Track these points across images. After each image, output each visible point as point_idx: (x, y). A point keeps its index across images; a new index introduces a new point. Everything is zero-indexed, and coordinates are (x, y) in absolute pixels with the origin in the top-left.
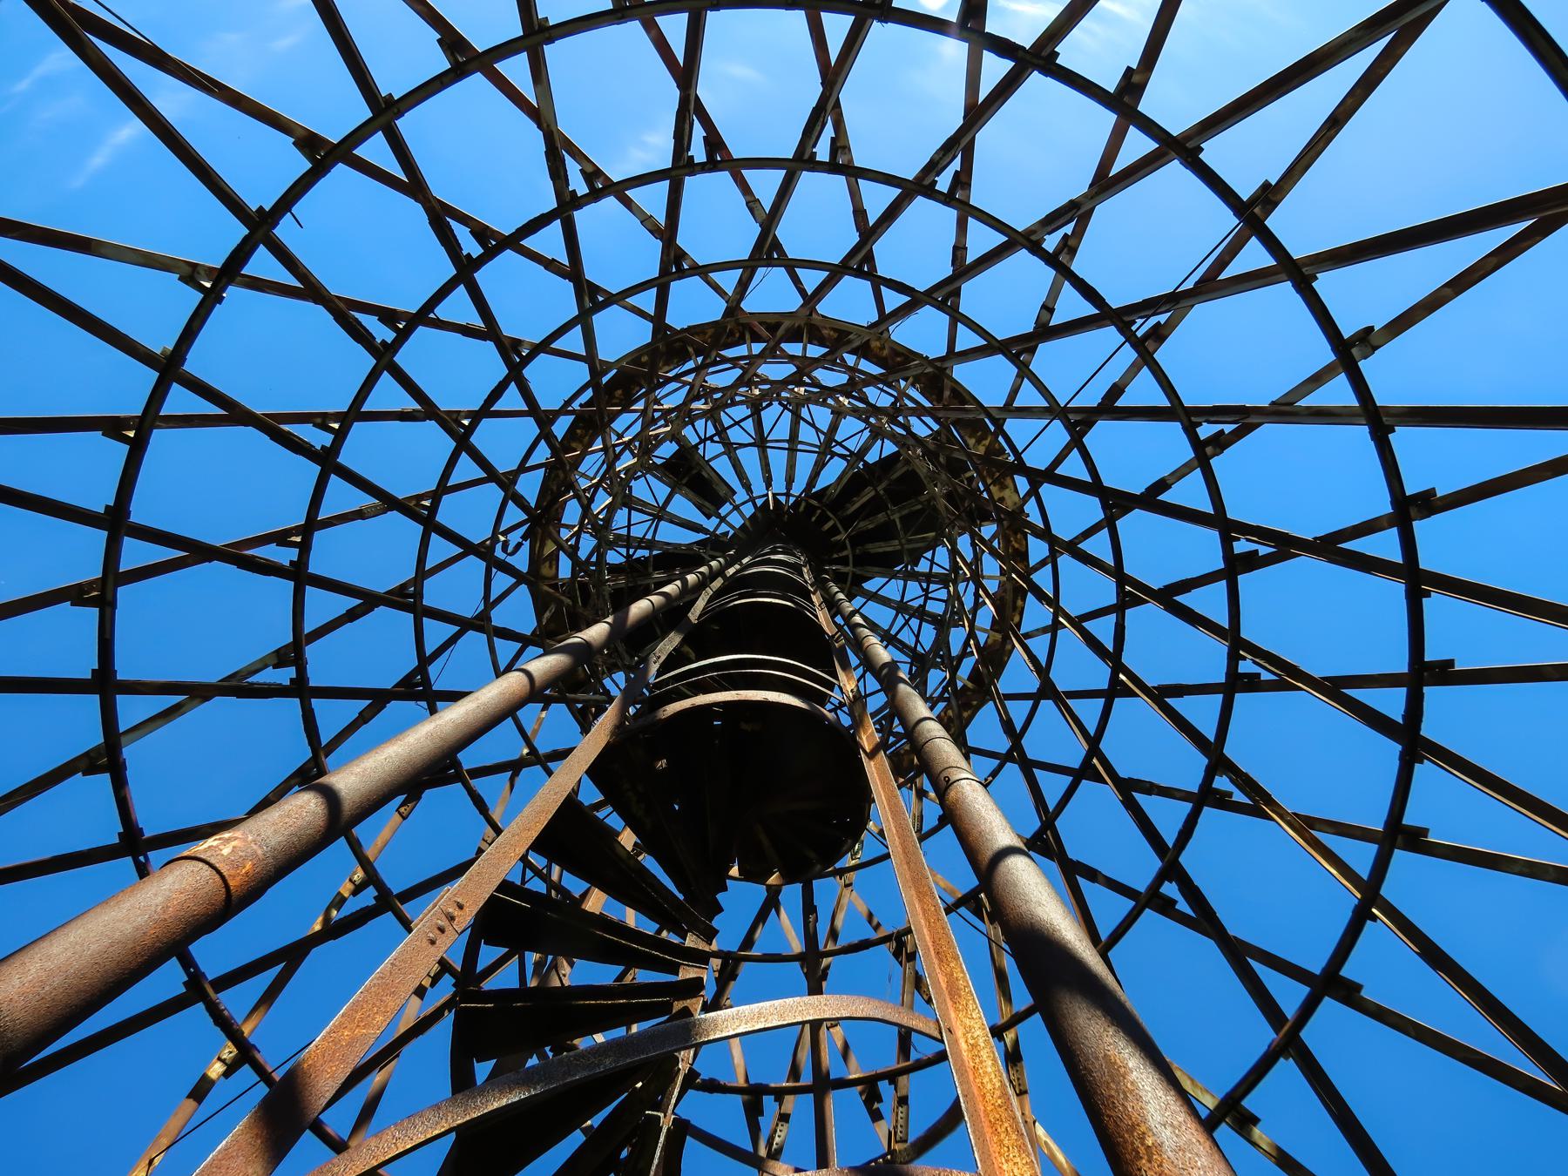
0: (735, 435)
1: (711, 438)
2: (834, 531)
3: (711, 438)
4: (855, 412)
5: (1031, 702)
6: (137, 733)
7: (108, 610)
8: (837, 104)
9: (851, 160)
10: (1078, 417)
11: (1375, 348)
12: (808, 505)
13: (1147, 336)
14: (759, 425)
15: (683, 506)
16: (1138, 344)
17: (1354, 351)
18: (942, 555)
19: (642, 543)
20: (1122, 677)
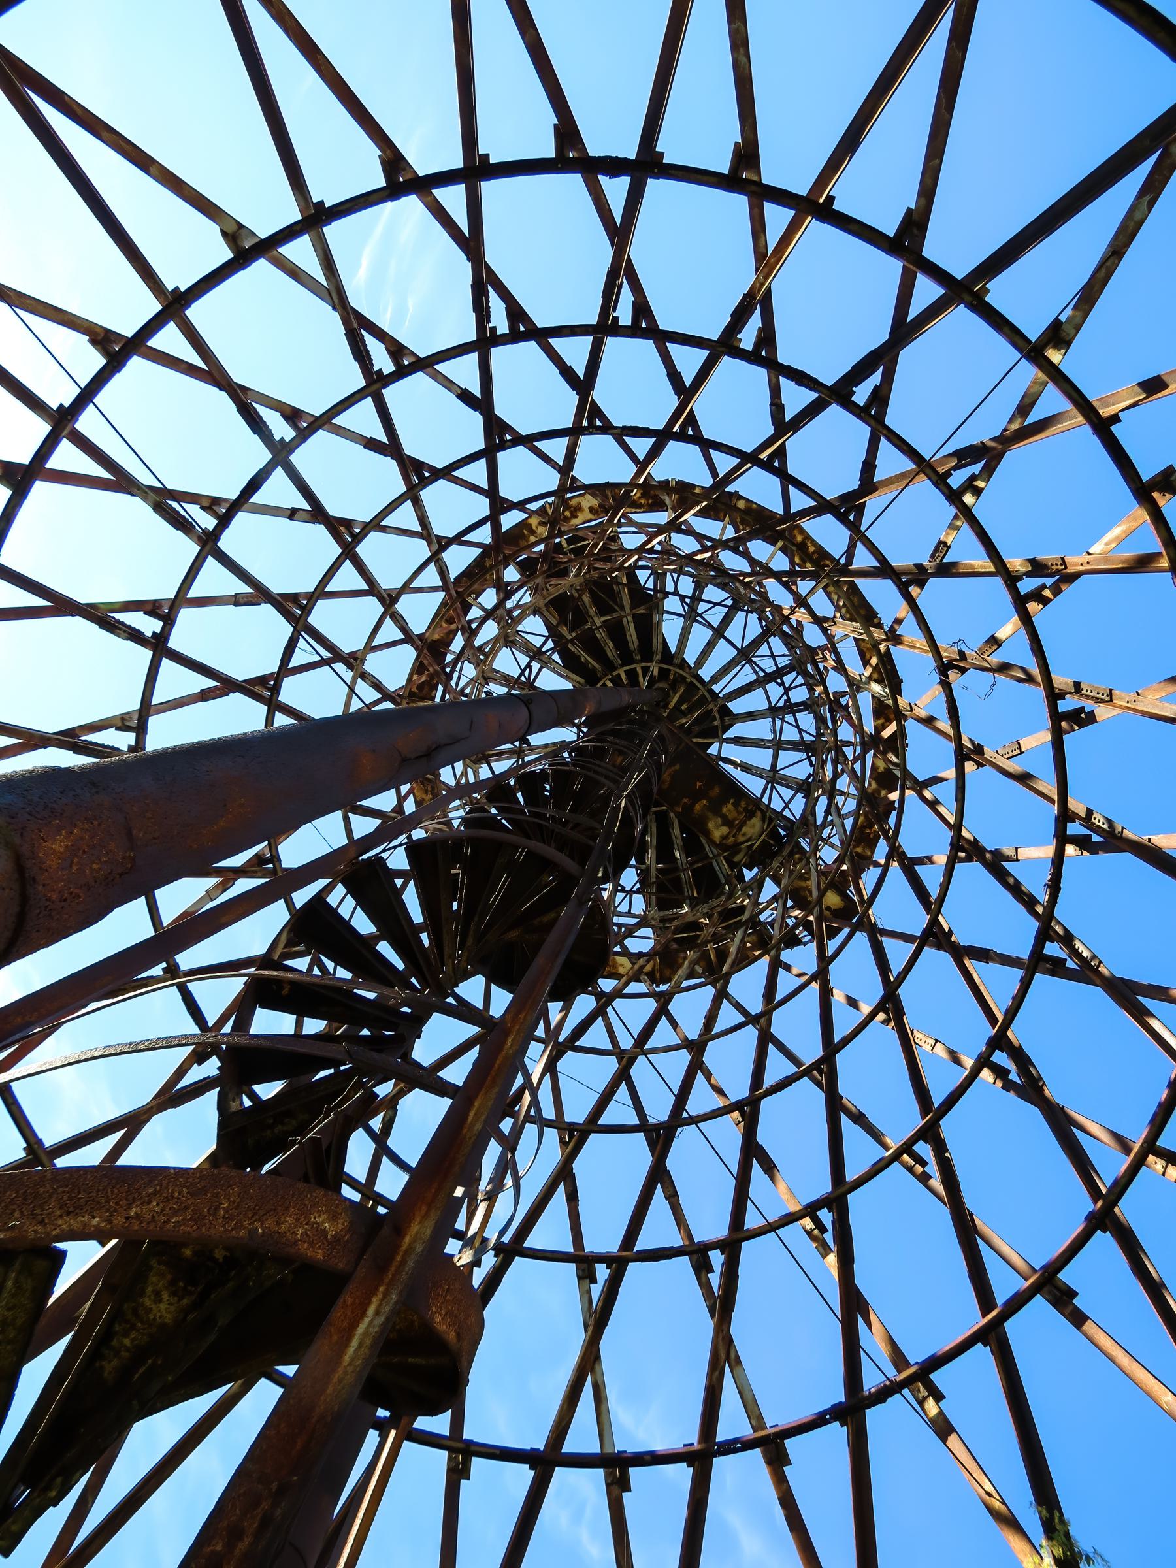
6: (606, 1427)
7: (473, 1448)
11: (241, 226)
17: (247, 245)
20: (676, 428)
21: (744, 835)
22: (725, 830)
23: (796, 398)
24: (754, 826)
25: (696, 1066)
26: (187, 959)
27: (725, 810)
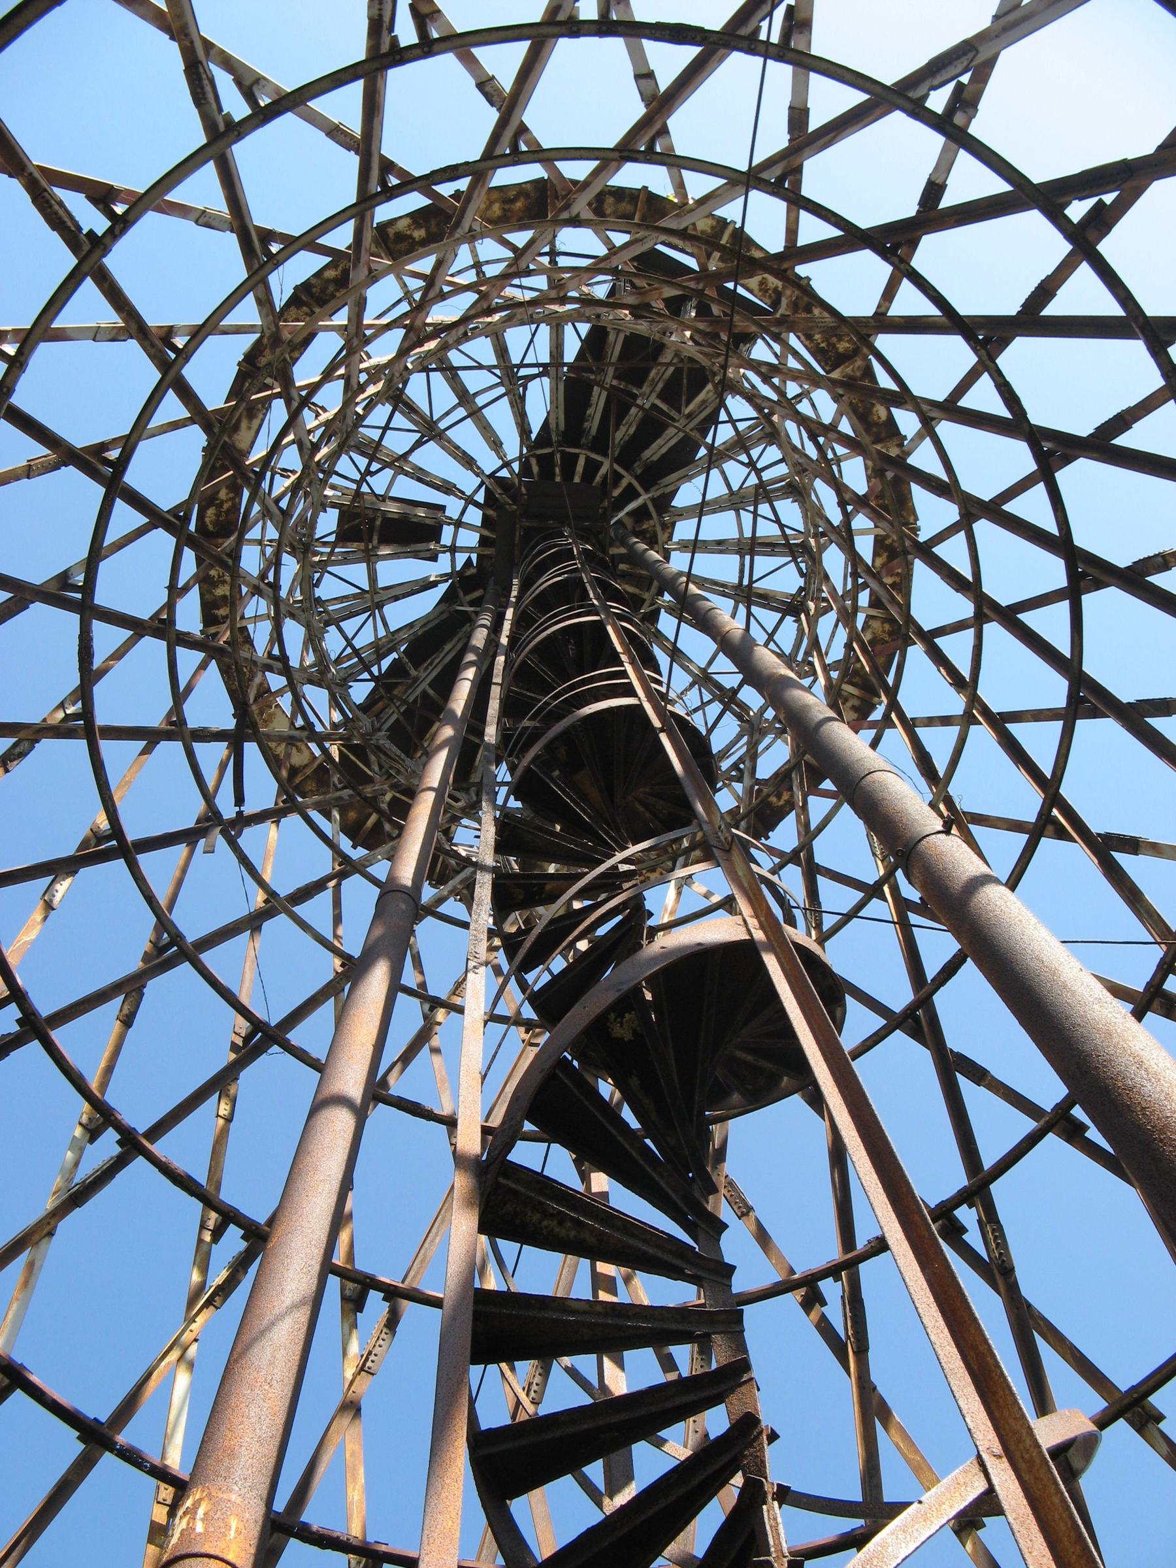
0: (397, 443)
1: (368, 472)
2: (592, 467)
3: (368, 472)
4: (509, 322)
5: (962, 535)
8: (208, 45)
9: (278, 89)
10: (777, 170)
12: (540, 458)
13: (786, 34)
14: (410, 409)
15: (395, 570)
16: (783, 52)
18: (738, 407)
19: (380, 649)
20: (1055, 812)
23: (202, 189)
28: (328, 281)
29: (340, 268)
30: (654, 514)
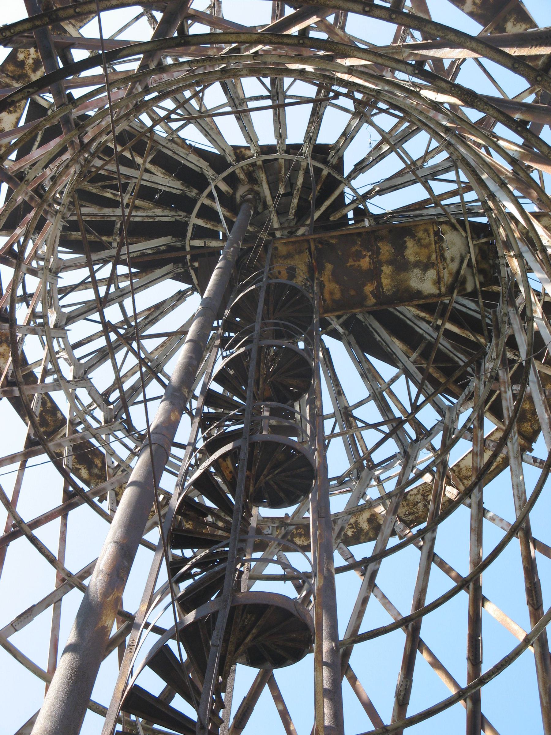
21: (452, 260)
22: (431, 274)
24: (453, 243)
25: (415, 644)
26: (454, 186)
27: (412, 259)
28: (90, 474)
29: (78, 466)
30: (229, 170)
